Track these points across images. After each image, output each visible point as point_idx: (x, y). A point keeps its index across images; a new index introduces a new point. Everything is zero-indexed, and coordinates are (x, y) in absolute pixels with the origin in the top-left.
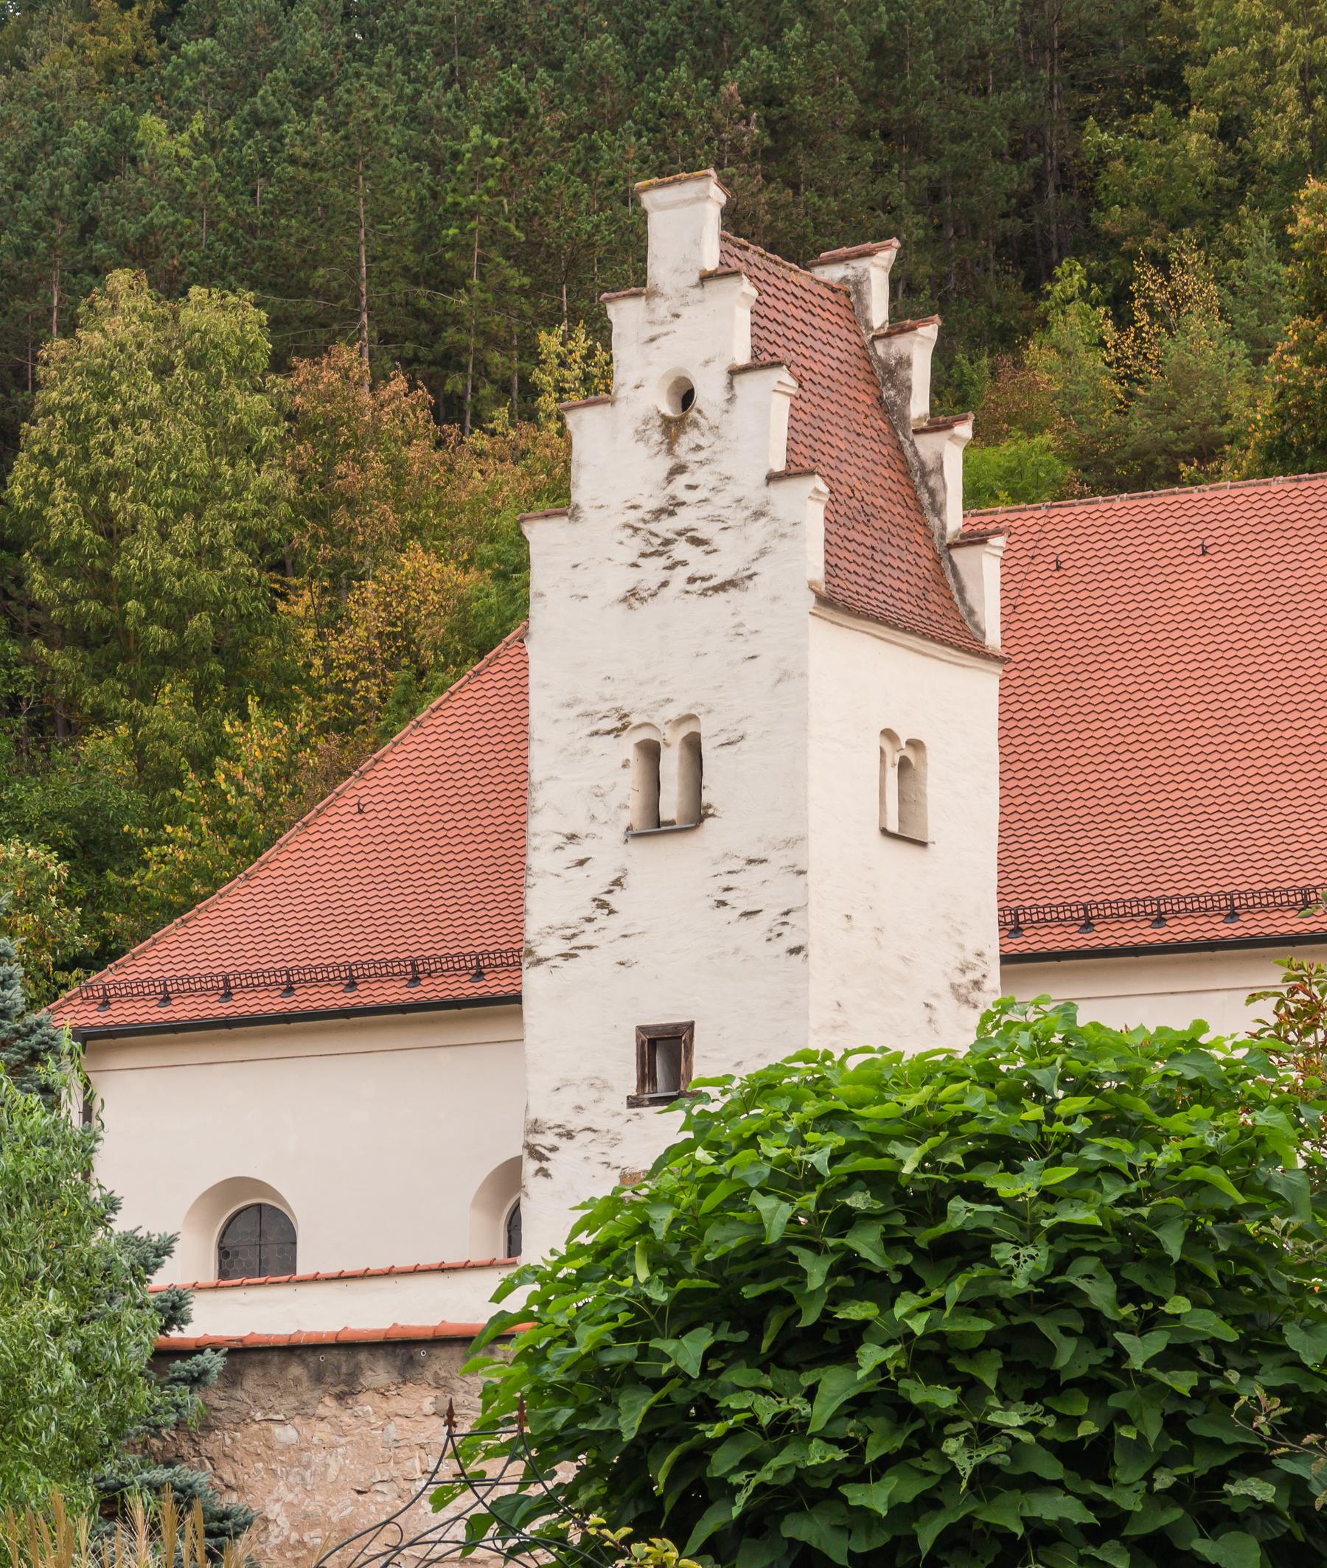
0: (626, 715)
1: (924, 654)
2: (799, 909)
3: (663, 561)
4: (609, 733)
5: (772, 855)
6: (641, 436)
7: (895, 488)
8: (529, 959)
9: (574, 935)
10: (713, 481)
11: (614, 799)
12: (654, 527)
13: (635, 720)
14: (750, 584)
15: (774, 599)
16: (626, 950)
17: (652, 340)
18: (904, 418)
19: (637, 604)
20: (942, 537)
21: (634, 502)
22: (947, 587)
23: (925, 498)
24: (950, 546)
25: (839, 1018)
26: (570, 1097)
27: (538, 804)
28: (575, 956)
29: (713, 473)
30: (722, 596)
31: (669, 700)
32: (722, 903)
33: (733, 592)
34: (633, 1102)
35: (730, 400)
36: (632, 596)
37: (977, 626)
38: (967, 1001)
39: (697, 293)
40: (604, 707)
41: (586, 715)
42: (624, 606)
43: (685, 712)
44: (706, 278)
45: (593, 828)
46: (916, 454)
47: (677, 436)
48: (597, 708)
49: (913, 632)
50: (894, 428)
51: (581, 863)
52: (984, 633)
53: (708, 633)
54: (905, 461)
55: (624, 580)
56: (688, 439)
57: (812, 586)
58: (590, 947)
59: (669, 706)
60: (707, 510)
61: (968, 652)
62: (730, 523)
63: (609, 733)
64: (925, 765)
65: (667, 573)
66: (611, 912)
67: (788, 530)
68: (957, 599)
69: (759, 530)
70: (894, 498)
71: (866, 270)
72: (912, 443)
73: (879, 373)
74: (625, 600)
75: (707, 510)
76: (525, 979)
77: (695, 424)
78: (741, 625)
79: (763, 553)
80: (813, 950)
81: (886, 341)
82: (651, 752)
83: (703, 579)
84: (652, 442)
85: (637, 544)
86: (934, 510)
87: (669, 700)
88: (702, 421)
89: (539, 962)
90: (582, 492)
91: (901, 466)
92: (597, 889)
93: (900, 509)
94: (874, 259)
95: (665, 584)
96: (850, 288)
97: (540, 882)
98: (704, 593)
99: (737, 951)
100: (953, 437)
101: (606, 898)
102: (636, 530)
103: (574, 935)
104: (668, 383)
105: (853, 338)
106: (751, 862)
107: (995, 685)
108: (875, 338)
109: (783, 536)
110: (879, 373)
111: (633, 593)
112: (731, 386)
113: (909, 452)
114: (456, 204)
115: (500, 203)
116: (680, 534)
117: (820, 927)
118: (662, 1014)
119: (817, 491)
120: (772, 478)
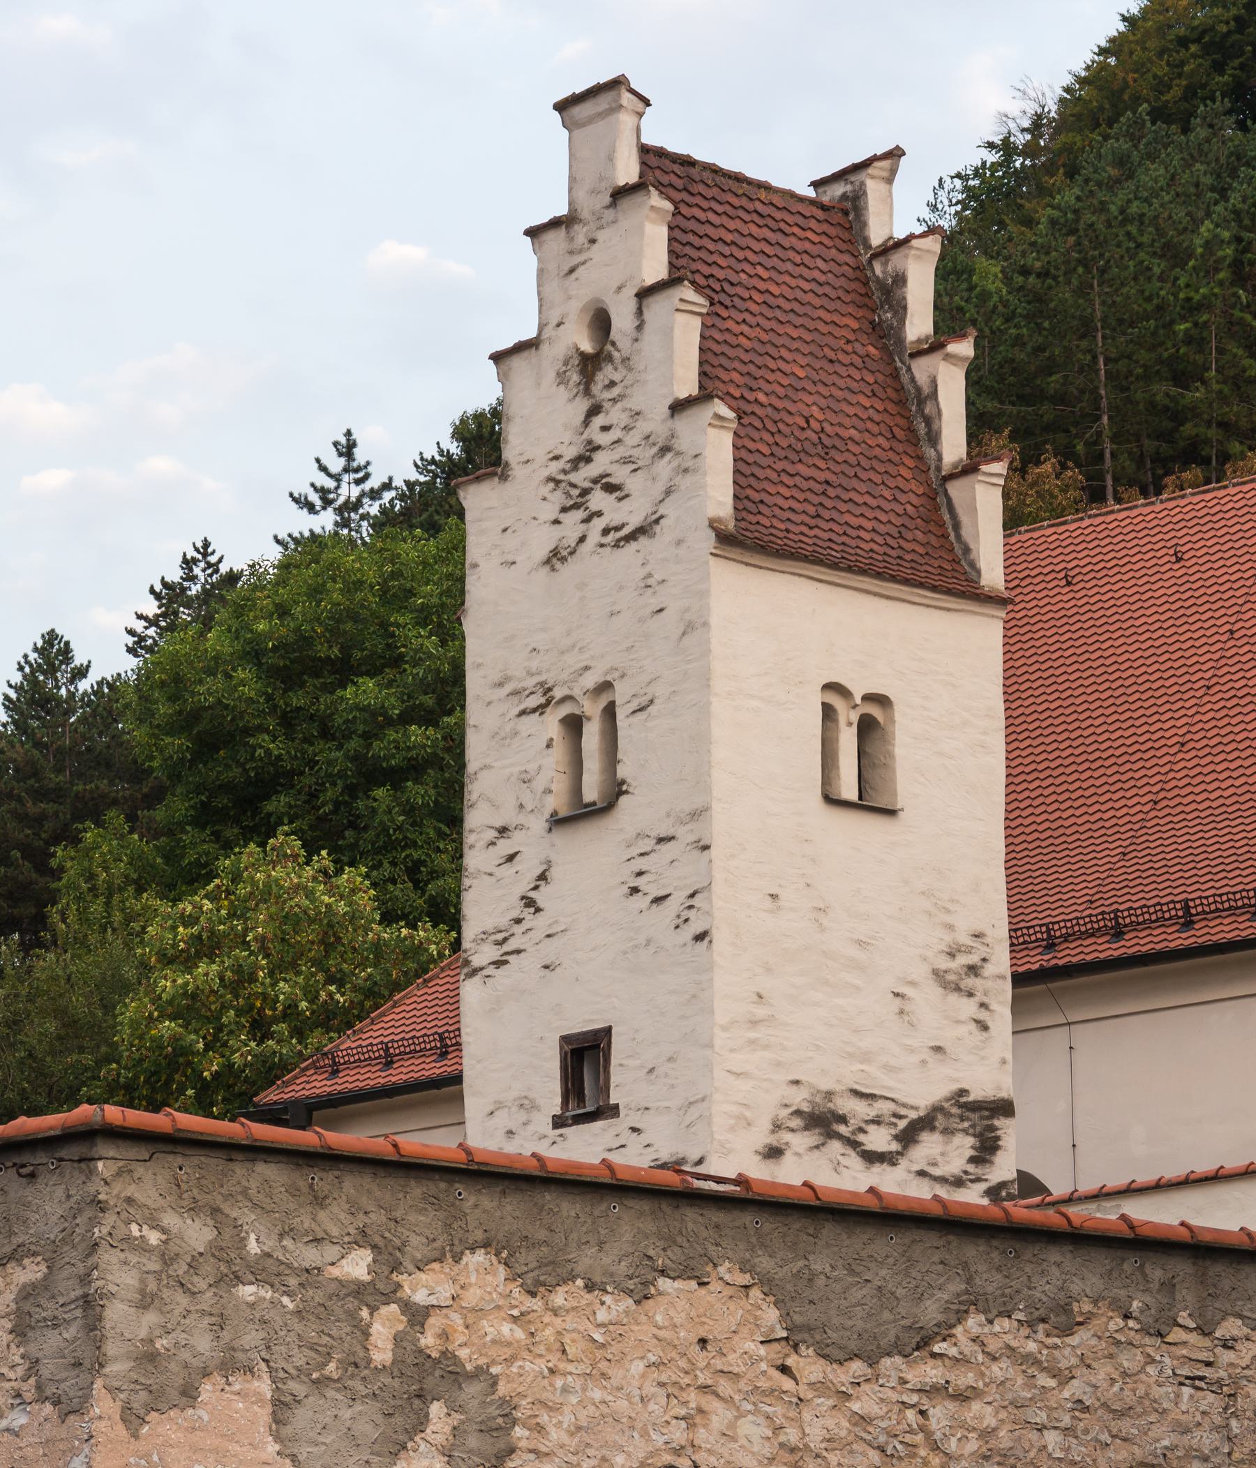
0: (550, 689)
1: (888, 598)
2: (704, 888)
3: (580, 514)
4: (534, 711)
5: (680, 831)
6: (562, 378)
7: (877, 417)
8: (465, 970)
9: (505, 940)
10: (624, 419)
11: (540, 784)
12: (575, 477)
13: (558, 693)
14: (657, 529)
15: (679, 542)
16: (550, 951)
17: (572, 271)
18: (900, 341)
19: (558, 565)
20: (939, 469)
21: (556, 452)
22: (942, 525)
23: (922, 428)
24: (952, 477)
25: (761, 1012)
26: (503, 1120)
27: (474, 797)
28: (506, 962)
29: (624, 410)
30: (634, 545)
31: (587, 668)
32: (635, 890)
33: (643, 540)
34: (558, 1122)
35: (639, 328)
36: (556, 557)
37: (973, 565)
38: (958, 989)
39: (609, 215)
40: (530, 683)
41: (515, 693)
42: (547, 568)
43: (602, 679)
44: (620, 194)
45: (521, 819)
46: (913, 379)
47: (593, 374)
48: (524, 684)
49: (863, 572)
50: (891, 355)
51: (511, 858)
52: (979, 572)
53: (621, 588)
54: (900, 389)
55: (543, 540)
56: (607, 373)
57: (713, 524)
58: (518, 952)
59: (588, 673)
60: (620, 452)
61: (962, 595)
62: (640, 463)
63: (534, 711)
64: (893, 722)
65: (584, 526)
66: (538, 910)
67: (690, 464)
68: (952, 537)
69: (665, 467)
70: (875, 429)
71: (863, 184)
72: (909, 369)
73: (877, 295)
74: (548, 561)
75: (620, 452)
76: (463, 991)
77: (610, 358)
78: (650, 575)
79: (668, 492)
80: (716, 935)
81: (883, 259)
82: (574, 725)
83: (617, 529)
84: (571, 383)
85: (558, 498)
86: (930, 440)
87: (587, 668)
88: (616, 354)
89: (475, 972)
90: (511, 452)
91: (893, 395)
92: (523, 887)
93: (881, 440)
94: (870, 171)
95: (582, 539)
96: (848, 205)
97: (475, 882)
98: (616, 545)
99: (648, 942)
100: (948, 357)
101: (532, 894)
102: (558, 482)
103: (505, 940)
104: (587, 317)
105: (847, 258)
106: (661, 840)
107: (999, 632)
108: (874, 256)
109: (686, 471)
110: (877, 295)
111: (555, 553)
112: (640, 312)
113: (905, 379)
114: (1189, 299)
115: (1235, 295)
116: (595, 481)
117: (727, 909)
118: (581, 1022)
119: (718, 417)
120: (678, 407)
